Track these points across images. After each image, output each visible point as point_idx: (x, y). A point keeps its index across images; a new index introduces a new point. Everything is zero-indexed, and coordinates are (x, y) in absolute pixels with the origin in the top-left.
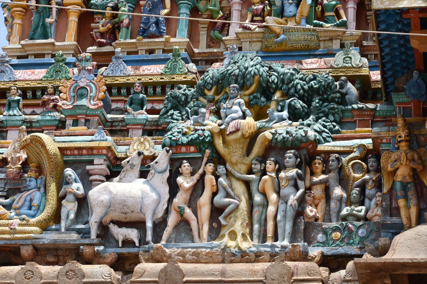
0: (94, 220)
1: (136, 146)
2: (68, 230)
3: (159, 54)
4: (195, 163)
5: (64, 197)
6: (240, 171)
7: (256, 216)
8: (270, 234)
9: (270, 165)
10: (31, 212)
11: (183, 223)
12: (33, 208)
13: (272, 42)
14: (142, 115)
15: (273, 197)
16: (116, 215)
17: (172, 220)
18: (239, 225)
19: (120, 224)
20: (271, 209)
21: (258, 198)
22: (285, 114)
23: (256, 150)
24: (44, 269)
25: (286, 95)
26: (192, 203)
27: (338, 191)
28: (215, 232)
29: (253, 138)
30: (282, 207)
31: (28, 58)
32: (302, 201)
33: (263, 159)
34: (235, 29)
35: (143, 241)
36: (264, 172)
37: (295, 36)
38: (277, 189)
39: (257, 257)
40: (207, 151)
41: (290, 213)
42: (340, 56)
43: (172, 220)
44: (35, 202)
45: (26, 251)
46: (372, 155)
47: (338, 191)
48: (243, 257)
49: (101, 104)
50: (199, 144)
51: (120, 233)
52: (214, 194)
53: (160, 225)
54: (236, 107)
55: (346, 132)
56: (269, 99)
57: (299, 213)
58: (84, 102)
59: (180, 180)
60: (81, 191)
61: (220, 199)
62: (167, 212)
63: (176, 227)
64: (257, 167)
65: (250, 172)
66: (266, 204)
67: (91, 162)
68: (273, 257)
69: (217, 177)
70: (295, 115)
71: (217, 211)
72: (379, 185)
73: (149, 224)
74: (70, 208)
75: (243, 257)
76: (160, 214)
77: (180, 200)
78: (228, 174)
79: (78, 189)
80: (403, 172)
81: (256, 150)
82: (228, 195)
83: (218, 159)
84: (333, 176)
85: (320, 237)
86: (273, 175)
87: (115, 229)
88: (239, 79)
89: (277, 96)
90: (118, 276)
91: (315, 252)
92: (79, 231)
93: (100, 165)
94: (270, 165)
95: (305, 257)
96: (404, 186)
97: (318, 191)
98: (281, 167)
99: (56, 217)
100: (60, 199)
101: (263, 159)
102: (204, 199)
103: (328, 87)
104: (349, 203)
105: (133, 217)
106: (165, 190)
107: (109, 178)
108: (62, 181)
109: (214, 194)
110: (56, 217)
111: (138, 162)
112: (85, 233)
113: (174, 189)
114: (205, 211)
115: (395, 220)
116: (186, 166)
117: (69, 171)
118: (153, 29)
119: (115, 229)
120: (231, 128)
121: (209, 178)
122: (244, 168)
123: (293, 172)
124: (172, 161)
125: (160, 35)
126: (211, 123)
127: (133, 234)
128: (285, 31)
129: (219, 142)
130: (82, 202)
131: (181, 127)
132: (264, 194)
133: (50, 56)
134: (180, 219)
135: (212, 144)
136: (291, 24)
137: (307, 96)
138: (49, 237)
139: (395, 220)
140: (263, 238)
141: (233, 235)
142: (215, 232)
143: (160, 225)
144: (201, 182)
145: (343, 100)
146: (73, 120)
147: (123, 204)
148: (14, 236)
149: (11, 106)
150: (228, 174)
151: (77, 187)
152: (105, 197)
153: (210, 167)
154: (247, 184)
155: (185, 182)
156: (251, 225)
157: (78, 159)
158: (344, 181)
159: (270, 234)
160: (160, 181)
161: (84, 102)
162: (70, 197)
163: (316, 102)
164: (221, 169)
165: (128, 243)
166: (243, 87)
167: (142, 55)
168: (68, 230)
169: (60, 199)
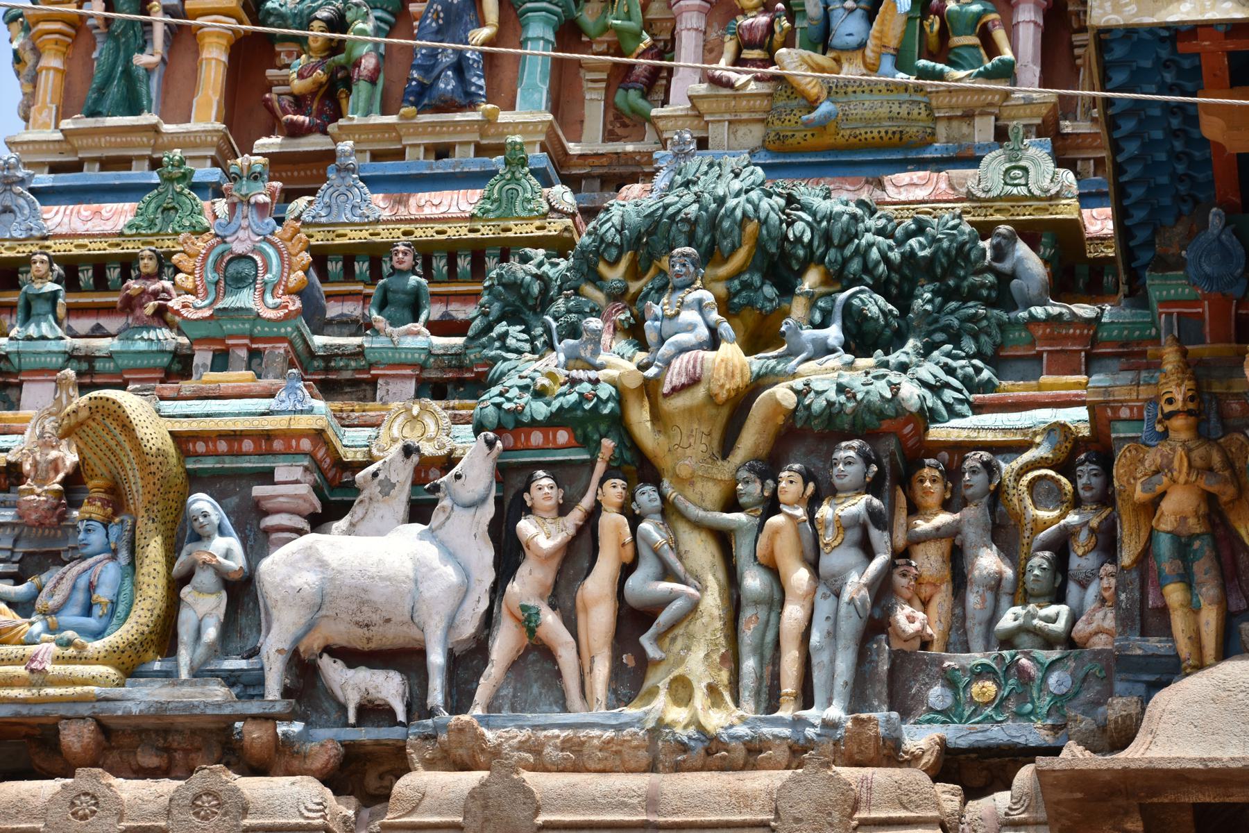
0: (274, 645)
1: (398, 427)
2: (199, 673)
3: (465, 160)
4: (570, 477)
5: (186, 579)
6: (701, 501)
7: (748, 634)
8: (789, 685)
9: (790, 484)
10: (92, 622)
11: (537, 655)
12: (97, 611)
13: (795, 123)
14: (416, 339)
15: (799, 577)
16: (341, 632)
17: (504, 644)
18: (698, 661)
19: (352, 657)
20: (793, 613)
21: (754, 581)
22: (834, 333)
23: (750, 440)
24: (128, 789)
25: (838, 278)
26: (562, 594)
27: (988, 561)
28: (630, 679)
29: (739, 405)
30: (824, 607)
31: (81, 170)
32: (883, 589)
33: (768, 467)
34: (686, 84)
35: (417, 706)
36: (772, 506)
37: (862, 107)
38: (810, 555)
39: (753, 754)
40: (605, 441)
41: (850, 626)
42: (994, 166)
43: (504, 644)
44: (104, 594)
45: (75, 737)
46: (1087, 456)
47: (988, 561)
48: (711, 753)
49: (296, 304)
50: (583, 422)
51: (350, 683)
52: (627, 569)
53: (467, 661)
54: (689, 313)
55: (1012, 389)
56: (787, 290)
57: (876, 624)
58: (245, 299)
59: (526, 527)
60: (238, 562)
61: (643, 584)
62: (489, 621)
63: (516, 666)
64: (752, 490)
65: (732, 503)
66: (777, 598)
67: (267, 477)
68: (797, 753)
69: (635, 520)
70: (862, 338)
71: (633, 619)
72: (1107, 544)
73: (436, 658)
74: (204, 610)
75: (711, 753)
76: (468, 628)
77: (526, 586)
78: (668, 511)
79: (227, 556)
80: (1178, 505)
81: (750, 440)
82: (667, 573)
83: (639, 467)
84: (973, 516)
85: (937, 695)
86: (800, 512)
87: (335, 673)
88: (700, 231)
89: (810, 281)
90: (345, 808)
91: (921, 738)
92: (231, 679)
93: (292, 484)
94: (790, 484)
95: (891, 753)
96: (1182, 546)
97: (929, 561)
98: (822, 490)
99: (165, 637)
100: (177, 584)
101: (768, 467)
102: (598, 585)
103: (960, 256)
104: (1021, 594)
105: (390, 636)
106: (483, 556)
107: (318, 522)
108: (182, 532)
109: (627, 569)
110: (165, 637)
111: (402, 474)
112: (248, 684)
113: (509, 554)
114: (599, 618)
115: (1155, 644)
116: (544, 488)
117: (201, 502)
118: (447, 84)
119: (335, 673)
120: (674, 376)
121: (612, 523)
122: (713, 492)
123: (857, 505)
124: (503, 472)
125: (469, 102)
126: (618, 362)
127: (388, 686)
128: (834, 90)
129: (640, 417)
130: (241, 592)
131: (530, 373)
132: (772, 570)
133: (147, 163)
134: (527, 641)
135: (619, 423)
136: (851, 71)
137: (898, 282)
138: (143, 696)
139: (1155, 644)
140: (771, 699)
141: (681, 690)
142: (630, 679)
143: (467, 661)
144: (588, 533)
145: (1003, 292)
146: (214, 351)
147: (361, 598)
148: (42, 692)
149: (34, 312)
150: (668, 511)
151: (225, 548)
152: (307, 579)
153: (614, 491)
154: (723, 539)
155: (541, 534)
156: (733, 659)
157: (227, 468)
158: (1005, 531)
159: (789, 685)
160: (468, 530)
161: (245, 299)
162: (205, 578)
163: (924, 300)
164: (647, 497)
165: (373, 712)
166: (710, 255)
167: (416, 162)
168: (199, 673)
169: (177, 584)
